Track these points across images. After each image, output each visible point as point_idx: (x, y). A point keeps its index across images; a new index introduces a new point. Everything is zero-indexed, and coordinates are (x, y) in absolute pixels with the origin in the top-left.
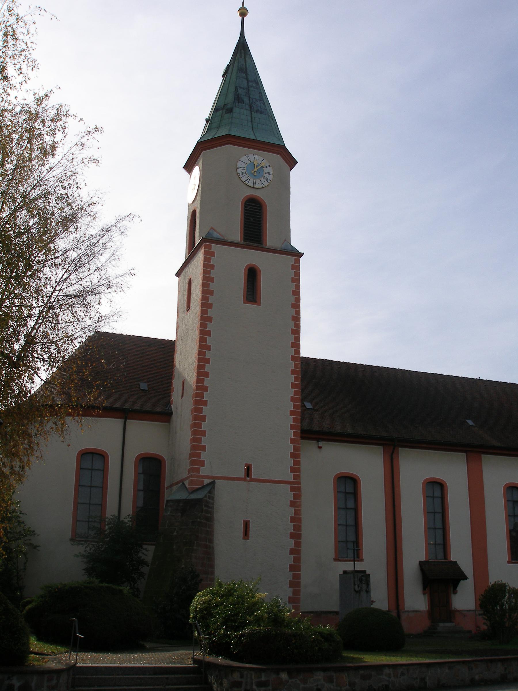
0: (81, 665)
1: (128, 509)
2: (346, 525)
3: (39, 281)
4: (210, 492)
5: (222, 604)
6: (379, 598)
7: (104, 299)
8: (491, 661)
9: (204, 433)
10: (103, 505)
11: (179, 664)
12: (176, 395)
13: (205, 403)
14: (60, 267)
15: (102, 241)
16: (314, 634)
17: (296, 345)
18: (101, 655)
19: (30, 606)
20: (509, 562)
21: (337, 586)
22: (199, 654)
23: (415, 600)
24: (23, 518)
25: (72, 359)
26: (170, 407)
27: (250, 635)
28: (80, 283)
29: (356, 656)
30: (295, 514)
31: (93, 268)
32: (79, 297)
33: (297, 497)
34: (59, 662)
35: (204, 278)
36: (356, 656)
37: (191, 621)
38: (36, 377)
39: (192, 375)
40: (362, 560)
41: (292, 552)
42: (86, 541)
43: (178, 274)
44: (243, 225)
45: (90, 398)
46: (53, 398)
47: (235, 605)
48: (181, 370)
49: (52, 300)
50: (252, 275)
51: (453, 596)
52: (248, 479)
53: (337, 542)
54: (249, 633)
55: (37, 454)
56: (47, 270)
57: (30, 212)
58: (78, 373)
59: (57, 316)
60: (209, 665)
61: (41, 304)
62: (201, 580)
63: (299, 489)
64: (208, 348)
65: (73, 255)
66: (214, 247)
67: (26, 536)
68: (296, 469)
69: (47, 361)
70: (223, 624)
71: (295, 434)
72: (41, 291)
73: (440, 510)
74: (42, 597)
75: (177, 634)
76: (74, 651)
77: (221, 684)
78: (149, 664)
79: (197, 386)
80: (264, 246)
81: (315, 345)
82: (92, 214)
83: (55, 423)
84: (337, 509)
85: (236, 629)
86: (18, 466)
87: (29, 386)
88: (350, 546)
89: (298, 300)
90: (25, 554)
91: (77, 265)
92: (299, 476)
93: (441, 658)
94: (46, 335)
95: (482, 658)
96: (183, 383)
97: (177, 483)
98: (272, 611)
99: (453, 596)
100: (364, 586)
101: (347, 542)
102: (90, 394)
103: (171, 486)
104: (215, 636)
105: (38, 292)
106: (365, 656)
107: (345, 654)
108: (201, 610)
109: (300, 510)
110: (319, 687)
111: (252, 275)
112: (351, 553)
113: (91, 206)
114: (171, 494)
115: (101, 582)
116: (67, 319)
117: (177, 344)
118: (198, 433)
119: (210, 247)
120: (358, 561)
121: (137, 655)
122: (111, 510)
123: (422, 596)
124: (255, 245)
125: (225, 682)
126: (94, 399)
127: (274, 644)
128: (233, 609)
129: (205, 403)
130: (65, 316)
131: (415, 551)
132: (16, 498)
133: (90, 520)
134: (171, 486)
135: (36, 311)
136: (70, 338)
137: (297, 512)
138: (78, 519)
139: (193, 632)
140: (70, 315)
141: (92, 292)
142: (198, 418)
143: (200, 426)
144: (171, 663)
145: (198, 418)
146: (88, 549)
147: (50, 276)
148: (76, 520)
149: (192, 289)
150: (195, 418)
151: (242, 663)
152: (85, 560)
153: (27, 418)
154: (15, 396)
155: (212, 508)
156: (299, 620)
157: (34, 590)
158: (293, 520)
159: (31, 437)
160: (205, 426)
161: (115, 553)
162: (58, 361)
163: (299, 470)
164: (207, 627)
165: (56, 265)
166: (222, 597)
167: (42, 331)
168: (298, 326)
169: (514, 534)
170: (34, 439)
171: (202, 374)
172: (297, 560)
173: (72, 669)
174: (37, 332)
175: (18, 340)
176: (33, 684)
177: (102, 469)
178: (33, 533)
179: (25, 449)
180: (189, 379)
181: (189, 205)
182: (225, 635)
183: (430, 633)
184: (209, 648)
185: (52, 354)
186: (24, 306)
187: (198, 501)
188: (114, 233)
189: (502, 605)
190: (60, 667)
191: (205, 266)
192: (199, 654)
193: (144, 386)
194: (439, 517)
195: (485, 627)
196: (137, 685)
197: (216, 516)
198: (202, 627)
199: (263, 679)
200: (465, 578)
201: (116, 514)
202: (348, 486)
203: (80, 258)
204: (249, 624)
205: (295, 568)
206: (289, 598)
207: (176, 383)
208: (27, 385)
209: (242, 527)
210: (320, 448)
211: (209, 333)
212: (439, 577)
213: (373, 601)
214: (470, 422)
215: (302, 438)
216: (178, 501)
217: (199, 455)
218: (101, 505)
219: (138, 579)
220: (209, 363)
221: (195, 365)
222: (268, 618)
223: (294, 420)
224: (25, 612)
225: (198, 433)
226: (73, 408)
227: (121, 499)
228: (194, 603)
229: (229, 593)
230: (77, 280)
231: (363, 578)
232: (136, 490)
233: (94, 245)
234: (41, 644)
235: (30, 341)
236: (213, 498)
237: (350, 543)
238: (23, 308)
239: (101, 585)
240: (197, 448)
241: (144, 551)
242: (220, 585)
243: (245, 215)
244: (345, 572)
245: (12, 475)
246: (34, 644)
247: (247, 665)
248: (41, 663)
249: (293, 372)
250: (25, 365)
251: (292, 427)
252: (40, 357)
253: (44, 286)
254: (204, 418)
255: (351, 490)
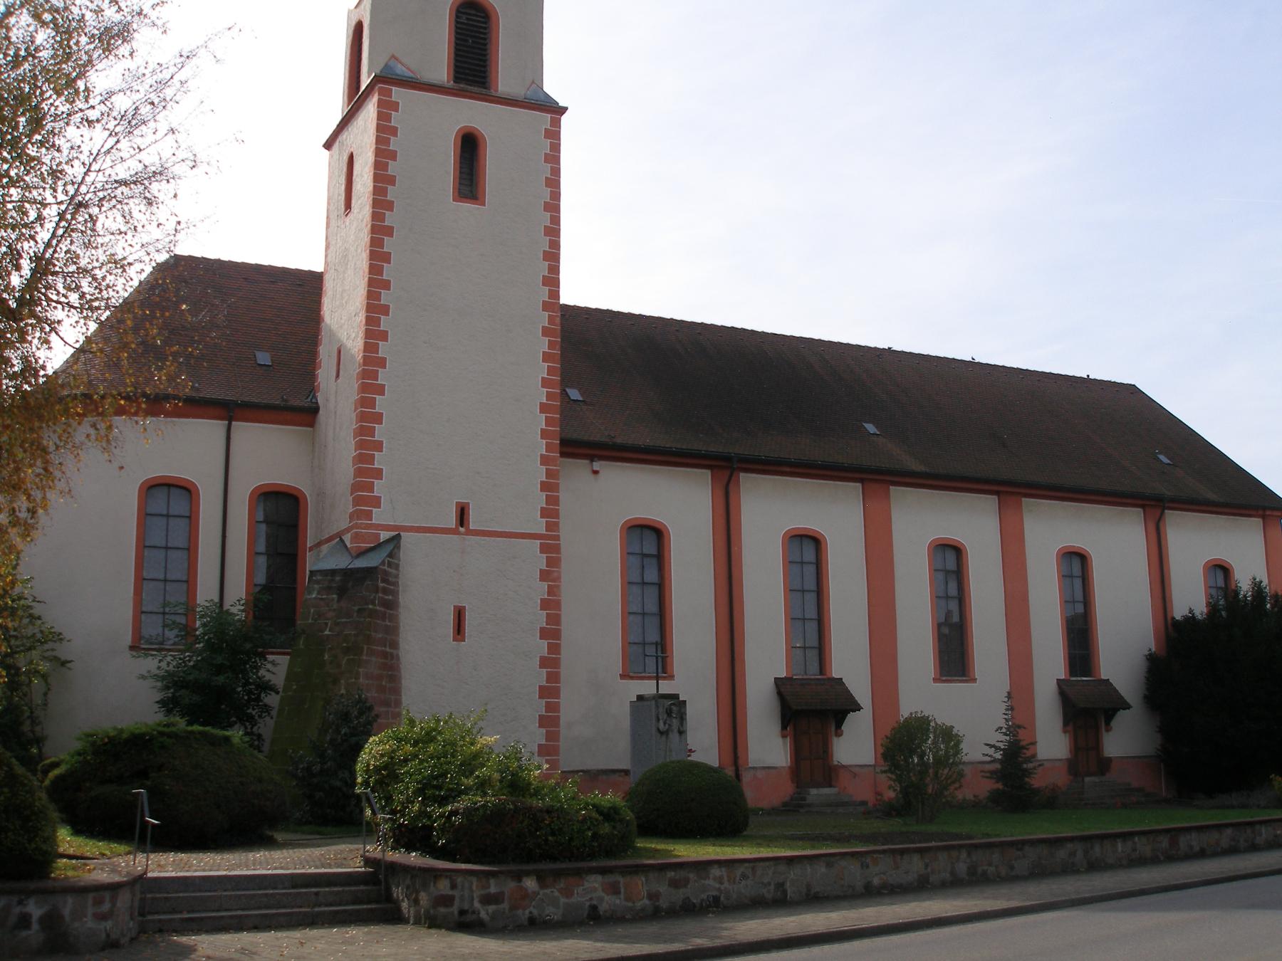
0: (155, 874)
1: (237, 591)
2: (644, 614)
3: (57, 154)
4: (391, 555)
5: (416, 756)
6: (703, 742)
7: (183, 187)
8: (903, 852)
9: (379, 446)
10: (190, 582)
11: (338, 867)
12: (325, 374)
13: (381, 390)
14: (98, 126)
15: (181, 76)
16: (585, 808)
17: (552, 281)
18: (194, 855)
19: (56, 772)
20: (935, 680)
21: (626, 723)
22: (373, 849)
23: (768, 748)
24: (37, 610)
25: (127, 304)
26: (315, 397)
27: (468, 812)
28: (139, 157)
29: (661, 846)
30: (549, 594)
31: (163, 127)
32: (135, 183)
33: (553, 562)
34: (114, 870)
35: (378, 152)
36: (661, 846)
37: (358, 791)
38: (53, 337)
39: (356, 337)
40: (671, 677)
41: (544, 662)
42: (159, 650)
43: (328, 145)
44: (453, 50)
45: (159, 379)
46: (90, 382)
47: (439, 759)
48: (334, 327)
49: (83, 189)
50: (470, 146)
51: (835, 740)
52: (462, 529)
53: (626, 644)
54: (467, 809)
55: (61, 485)
56: (71, 132)
57: (37, 16)
58: (136, 329)
59: (93, 219)
60: (393, 868)
61: (61, 197)
62: (377, 716)
63: (557, 549)
64: (386, 285)
65: (122, 103)
66: (398, 93)
67: (46, 642)
68: (550, 512)
69: (75, 308)
70: (419, 792)
71: (549, 447)
72: (61, 172)
73: (813, 587)
74: (79, 754)
75: (334, 813)
76: (143, 852)
77: (416, 901)
78: (282, 868)
79: (364, 357)
80: (493, 93)
81: (588, 283)
82: (159, 23)
83: (94, 426)
84: (627, 584)
85: (442, 801)
86: (24, 509)
87: (42, 354)
88: (651, 650)
89: (556, 196)
90: (44, 677)
91: (132, 121)
92: (557, 524)
93: (813, 847)
94: (73, 258)
95: (886, 847)
96: (339, 352)
97: (330, 539)
98: (508, 768)
99: (835, 740)
100: (675, 722)
101: (644, 644)
102: (160, 369)
103: (319, 544)
104: (403, 816)
105: (56, 174)
106: (677, 847)
107: (640, 844)
108: (378, 769)
109: (558, 586)
110: (595, 902)
111: (470, 146)
112: (651, 663)
113: (158, 8)
114: (320, 559)
115: (190, 723)
116: (114, 227)
117: (326, 277)
118: (367, 445)
119: (389, 94)
120: (664, 678)
121: (260, 855)
122: (206, 592)
123: (780, 740)
124: (476, 89)
125: (424, 898)
126: (168, 380)
127: (510, 840)
128: (435, 766)
129: (381, 390)
130: (109, 220)
131: (767, 658)
132: (23, 573)
133: (167, 610)
134: (319, 544)
135: (51, 212)
136: (119, 264)
137: (551, 591)
138: (144, 609)
139: (362, 811)
140: (119, 219)
141: (161, 174)
142: (368, 418)
143: (372, 432)
144: (323, 866)
145: (368, 418)
146: (164, 664)
147: (79, 143)
148: (139, 612)
149: (355, 173)
150: (362, 417)
151: (455, 861)
152: (159, 684)
153: (41, 418)
154: (13, 376)
155: (396, 584)
156: (557, 784)
157: (63, 744)
158: (545, 605)
159: (47, 453)
160: (380, 432)
161: (213, 675)
162: (98, 308)
163: (555, 514)
164: (389, 799)
165: (90, 123)
166: (416, 744)
167: (65, 249)
168: (555, 245)
169: (946, 630)
170: (53, 457)
171: (374, 334)
172: (554, 677)
173: (140, 881)
174: (55, 251)
175: (18, 268)
176: (66, 912)
177: (185, 578)
178: (58, 637)
179: (38, 475)
180: (349, 344)
181: (350, 12)
182: (422, 814)
183: (793, 807)
184: (394, 836)
185: (84, 294)
186: (28, 202)
187: (370, 572)
188: (203, 59)
189: (921, 757)
190: (117, 879)
191: (379, 128)
192: (373, 849)
193: (264, 358)
194: (811, 598)
195: (892, 794)
196: (259, 908)
197: (402, 599)
198: (380, 799)
199: (493, 890)
200: (857, 708)
201: (217, 599)
202: (647, 542)
203: (137, 108)
204: (465, 792)
205: (550, 692)
206: (540, 746)
207: (325, 353)
208: (38, 354)
209: (451, 618)
210: (596, 472)
211: (386, 258)
212: (812, 709)
213: (690, 751)
214: (871, 428)
215: (563, 454)
216: (333, 572)
217: (370, 487)
218: (189, 517)
219: (260, 716)
220: (394, 159)
221: (362, 317)
222: (501, 781)
223: (549, 396)
224: (47, 782)
225: (367, 445)
226: (127, 398)
227: (225, 572)
228: (364, 756)
229: (429, 737)
230: (132, 152)
231: (674, 707)
232: (252, 554)
233: (163, 84)
234: (80, 840)
235: (42, 267)
236: (397, 567)
237: (650, 646)
238: (27, 205)
239: (190, 728)
240: (366, 472)
241: (269, 666)
242: (412, 723)
243: (457, 33)
244: (640, 698)
245: (14, 526)
246: (66, 839)
247: (463, 866)
248: (80, 873)
249: (546, 332)
250: (33, 315)
251: (544, 434)
252: (63, 299)
253: (67, 163)
254: (378, 418)
255: (654, 551)
